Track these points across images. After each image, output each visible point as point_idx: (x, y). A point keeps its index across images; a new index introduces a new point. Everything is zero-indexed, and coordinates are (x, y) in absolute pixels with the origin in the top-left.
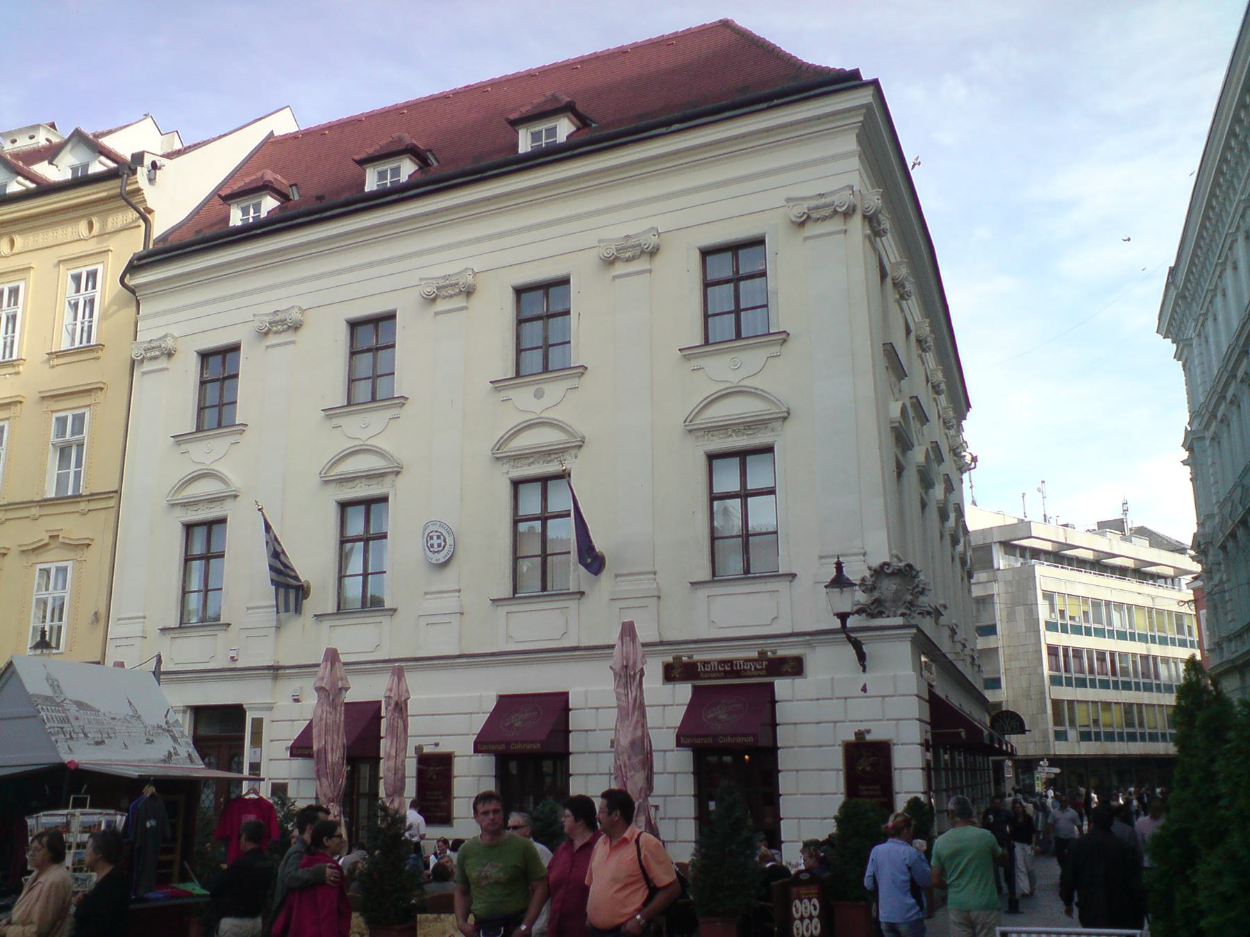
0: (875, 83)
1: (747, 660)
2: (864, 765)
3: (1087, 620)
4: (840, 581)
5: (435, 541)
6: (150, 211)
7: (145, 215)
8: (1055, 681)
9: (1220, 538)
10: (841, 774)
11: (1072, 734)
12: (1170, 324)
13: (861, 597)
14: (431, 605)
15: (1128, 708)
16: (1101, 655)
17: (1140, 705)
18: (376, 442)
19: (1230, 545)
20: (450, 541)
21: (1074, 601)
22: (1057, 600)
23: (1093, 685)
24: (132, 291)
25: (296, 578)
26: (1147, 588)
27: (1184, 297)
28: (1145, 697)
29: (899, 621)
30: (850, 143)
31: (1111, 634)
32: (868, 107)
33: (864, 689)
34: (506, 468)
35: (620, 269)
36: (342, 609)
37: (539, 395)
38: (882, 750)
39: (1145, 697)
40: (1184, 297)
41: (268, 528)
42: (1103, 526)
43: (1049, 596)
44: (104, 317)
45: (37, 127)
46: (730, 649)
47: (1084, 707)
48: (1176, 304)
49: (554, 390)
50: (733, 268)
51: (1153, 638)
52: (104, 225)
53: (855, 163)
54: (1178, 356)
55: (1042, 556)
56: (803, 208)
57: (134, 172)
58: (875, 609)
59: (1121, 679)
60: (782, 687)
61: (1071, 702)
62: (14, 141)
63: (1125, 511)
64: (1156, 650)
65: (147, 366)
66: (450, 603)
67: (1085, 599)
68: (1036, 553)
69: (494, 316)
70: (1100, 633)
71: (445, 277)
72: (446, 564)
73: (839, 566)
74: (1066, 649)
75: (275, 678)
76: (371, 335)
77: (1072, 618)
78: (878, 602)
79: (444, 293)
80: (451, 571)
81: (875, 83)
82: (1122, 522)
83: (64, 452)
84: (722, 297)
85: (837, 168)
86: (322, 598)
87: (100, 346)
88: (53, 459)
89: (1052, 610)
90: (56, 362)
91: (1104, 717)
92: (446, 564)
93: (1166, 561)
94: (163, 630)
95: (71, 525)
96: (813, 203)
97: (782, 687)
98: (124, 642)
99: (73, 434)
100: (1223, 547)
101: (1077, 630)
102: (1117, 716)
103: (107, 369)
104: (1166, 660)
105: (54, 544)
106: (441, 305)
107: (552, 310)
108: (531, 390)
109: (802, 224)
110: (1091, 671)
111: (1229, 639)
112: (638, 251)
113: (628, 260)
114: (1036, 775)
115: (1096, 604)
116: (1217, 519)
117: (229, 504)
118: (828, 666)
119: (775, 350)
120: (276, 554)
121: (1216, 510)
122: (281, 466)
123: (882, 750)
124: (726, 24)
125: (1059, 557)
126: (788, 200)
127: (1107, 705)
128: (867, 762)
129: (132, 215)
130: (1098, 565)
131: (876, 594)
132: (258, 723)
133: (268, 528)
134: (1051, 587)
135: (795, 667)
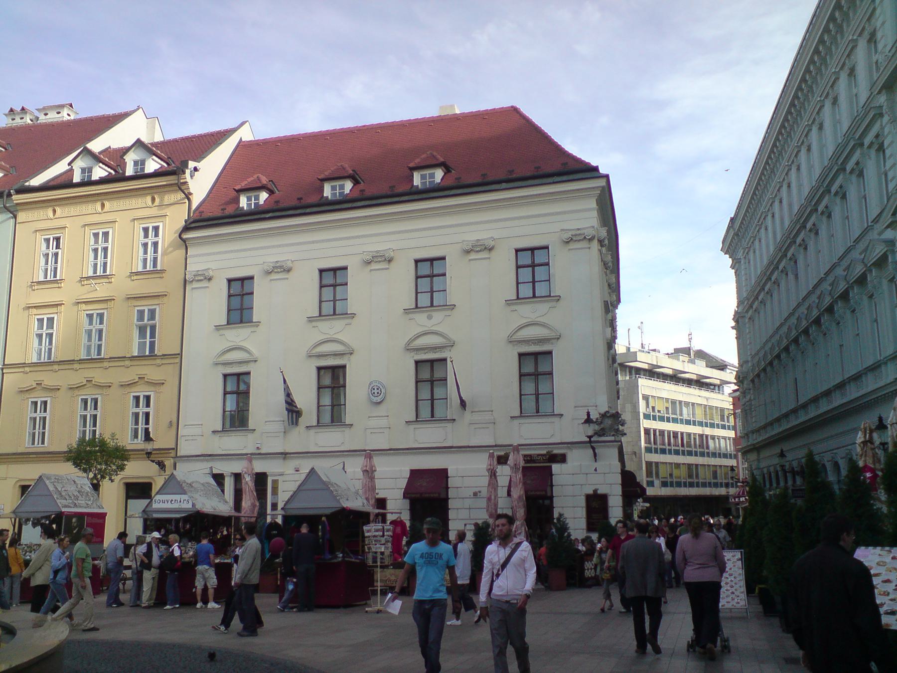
0: (607, 176)
1: (538, 455)
2: (595, 504)
3: (668, 413)
4: (588, 421)
5: (376, 391)
6: (191, 194)
7: (188, 196)
8: (648, 450)
9: (751, 376)
10: (584, 509)
11: (657, 483)
12: (729, 247)
13: (597, 427)
14: (373, 423)
15: (689, 466)
16: (675, 434)
17: (697, 465)
18: (339, 337)
19: (756, 380)
20: (383, 391)
21: (661, 401)
22: (650, 399)
23: (670, 453)
24: (184, 241)
25: (296, 407)
26: (704, 393)
27: (738, 235)
28: (700, 460)
29: (613, 438)
30: (593, 204)
31: (682, 421)
32: (603, 187)
33: (596, 470)
34: (412, 354)
35: (473, 256)
36: (319, 424)
37: (430, 317)
38: (604, 498)
39: (700, 460)
40: (738, 235)
41: (285, 381)
42: (678, 351)
43: (646, 398)
44: (164, 253)
45: (62, 106)
46: (534, 449)
47: (664, 466)
48: (733, 238)
49: (438, 316)
50: (532, 261)
51: (706, 423)
52: (162, 200)
53: (595, 214)
54: (732, 267)
55: (642, 373)
56: (569, 235)
57: (184, 173)
58: (601, 433)
59: (686, 449)
60: (556, 468)
61: (657, 463)
62: (46, 114)
63: (690, 340)
64: (708, 431)
65: (195, 285)
66: (383, 422)
67: (667, 400)
68: (638, 371)
69: (402, 276)
70: (675, 421)
71: (377, 252)
72: (380, 403)
73: (588, 414)
74: (655, 431)
75: (284, 458)
76: (332, 278)
77: (659, 411)
78: (603, 429)
79: (375, 260)
80: (383, 406)
81: (607, 176)
82: (689, 349)
83: (142, 330)
84: (424, 284)
85: (586, 218)
86: (309, 417)
87: (163, 271)
88: (136, 333)
89: (647, 406)
90: (135, 277)
91: (676, 472)
92: (380, 403)
93: (715, 375)
94: (214, 432)
95: (151, 372)
96: (574, 233)
97: (556, 468)
98: (191, 438)
99: (148, 320)
100: (753, 381)
101: (662, 419)
102: (683, 473)
103: (170, 283)
104: (713, 438)
105: (142, 382)
106: (374, 266)
107: (435, 272)
108: (425, 315)
109: (568, 242)
110: (669, 444)
111: (753, 432)
112: (483, 247)
113: (478, 252)
114: (635, 507)
115: (674, 402)
116: (750, 364)
117: (252, 364)
118: (578, 459)
119: (554, 304)
120: (288, 395)
121: (749, 359)
122: (282, 346)
123: (604, 498)
124: (515, 110)
125: (652, 373)
126: (562, 230)
127: (678, 465)
128: (596, 504)
129: (180, 195)
130: (675, 378)
131: (602, 426)
132: (275, 482)
133: (285, 381)
134: (647, 392)
135: (562, 459)
